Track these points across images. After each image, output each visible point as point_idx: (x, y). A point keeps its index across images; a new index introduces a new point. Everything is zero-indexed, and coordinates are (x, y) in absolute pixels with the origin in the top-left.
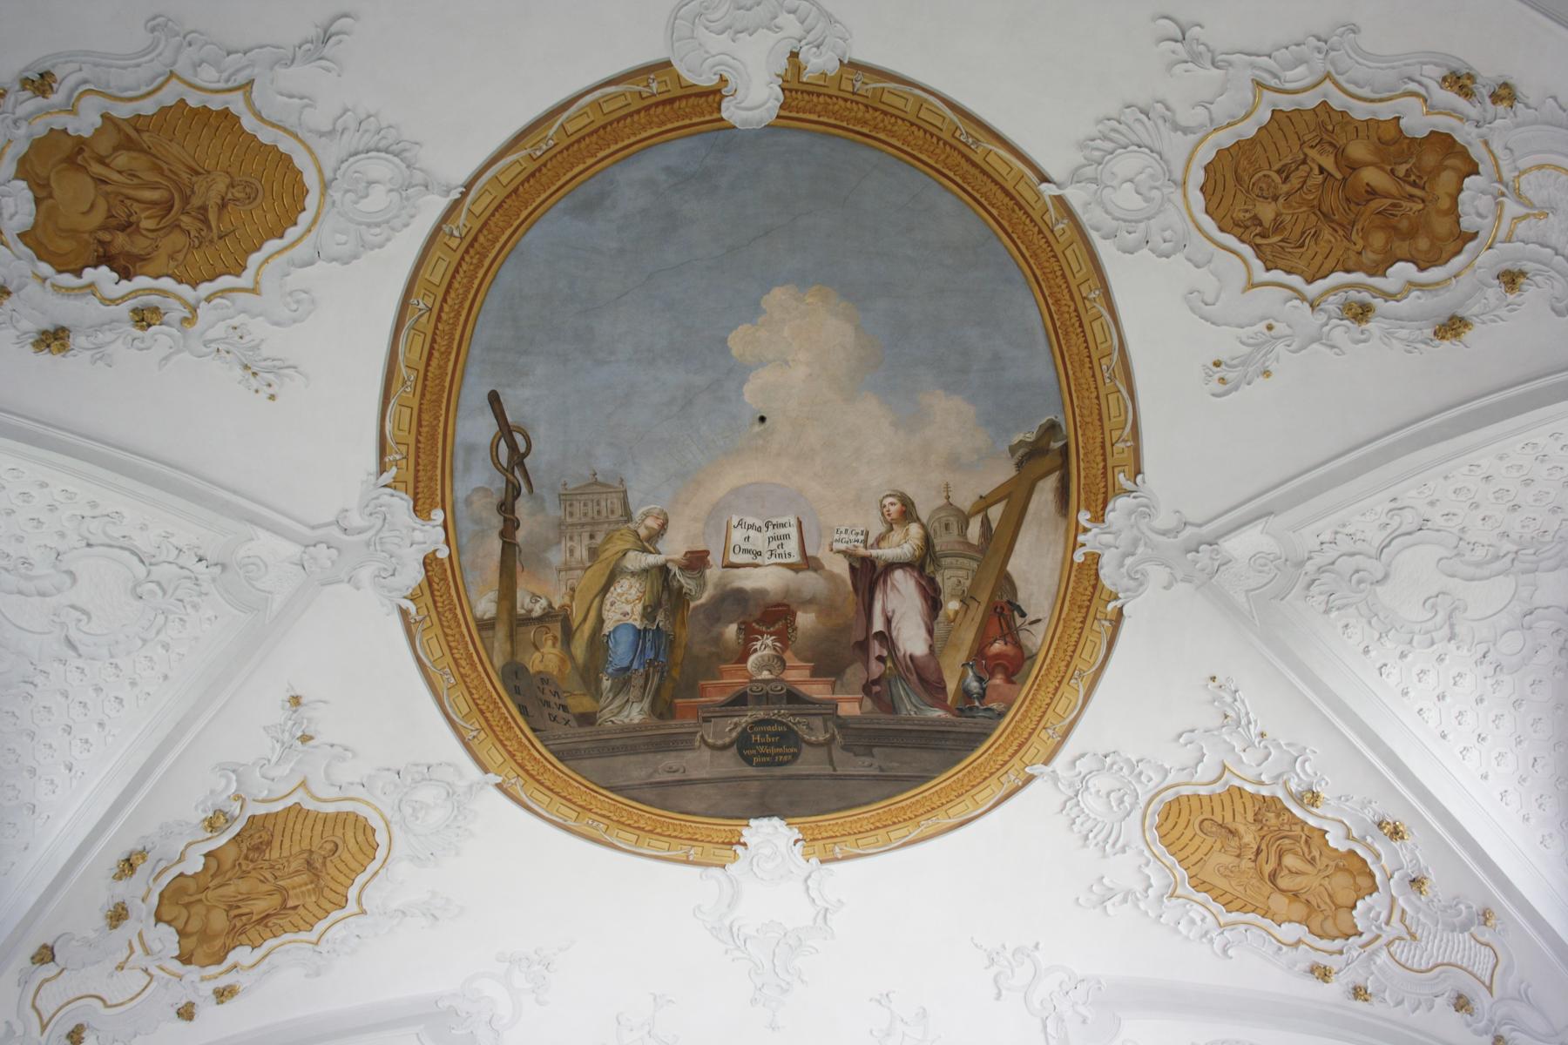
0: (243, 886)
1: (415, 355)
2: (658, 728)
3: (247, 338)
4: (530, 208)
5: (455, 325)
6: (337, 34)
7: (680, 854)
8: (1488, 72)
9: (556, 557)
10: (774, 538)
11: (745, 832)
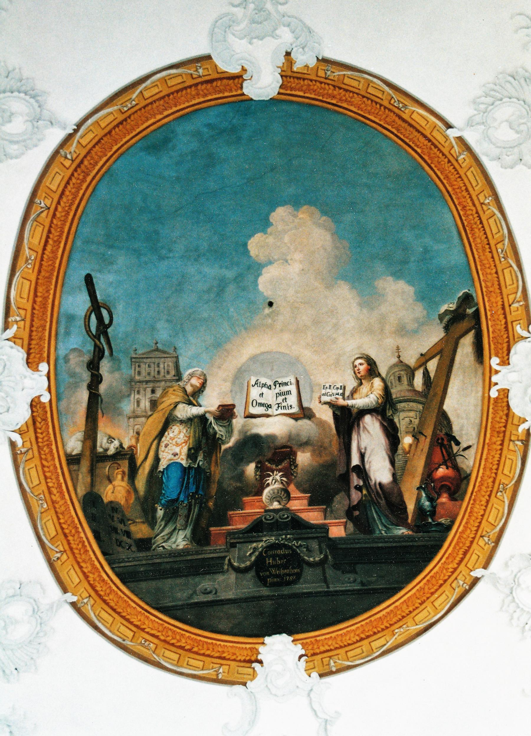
1: (36, 241)
2: (197, 553)
4: (119, 145)
5: (65, 221)
11: (261, 649)
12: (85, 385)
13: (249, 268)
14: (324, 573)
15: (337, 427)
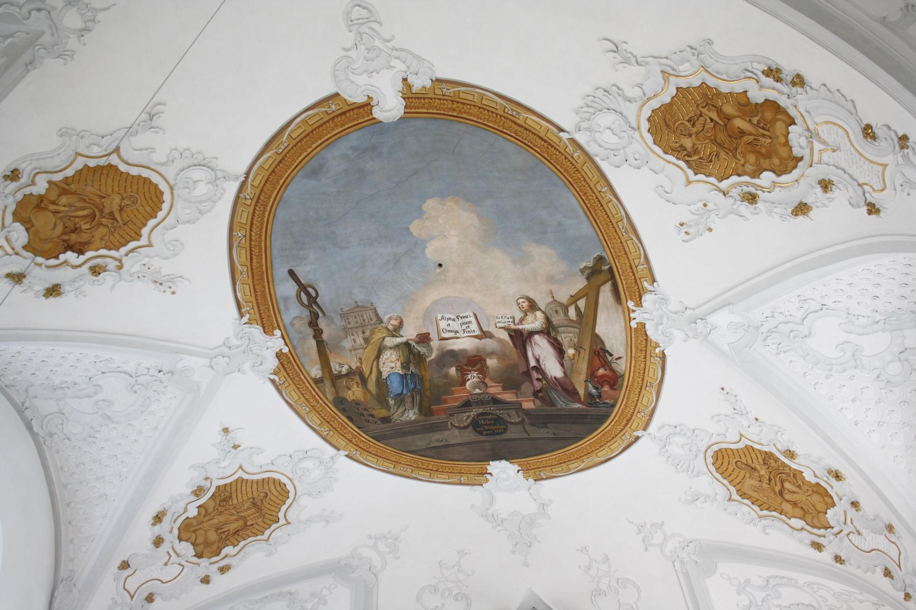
0: (222, 518)
1: (243, 259)
2: (426, 421)
3: (152, 269)
5: (260, 241)
6: (156, 114)
7: (455, 480)
8: (789, 69)
9: (347, 344)
10: (463, 324)
11: (488, 467)
12: (311, 338)
13: (416, 243)
14: (524, 427)
15: (514, 344)
